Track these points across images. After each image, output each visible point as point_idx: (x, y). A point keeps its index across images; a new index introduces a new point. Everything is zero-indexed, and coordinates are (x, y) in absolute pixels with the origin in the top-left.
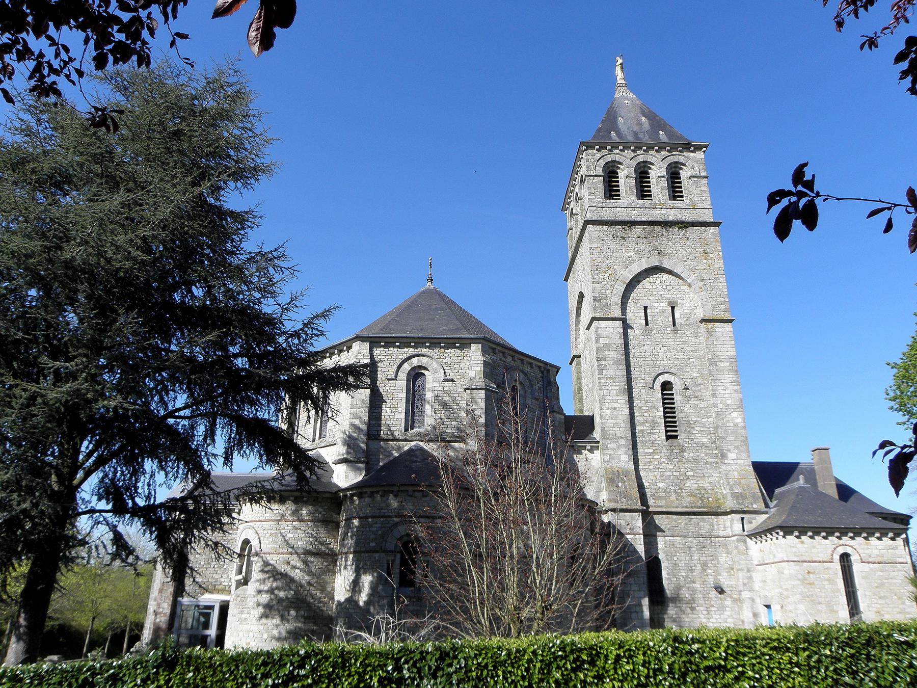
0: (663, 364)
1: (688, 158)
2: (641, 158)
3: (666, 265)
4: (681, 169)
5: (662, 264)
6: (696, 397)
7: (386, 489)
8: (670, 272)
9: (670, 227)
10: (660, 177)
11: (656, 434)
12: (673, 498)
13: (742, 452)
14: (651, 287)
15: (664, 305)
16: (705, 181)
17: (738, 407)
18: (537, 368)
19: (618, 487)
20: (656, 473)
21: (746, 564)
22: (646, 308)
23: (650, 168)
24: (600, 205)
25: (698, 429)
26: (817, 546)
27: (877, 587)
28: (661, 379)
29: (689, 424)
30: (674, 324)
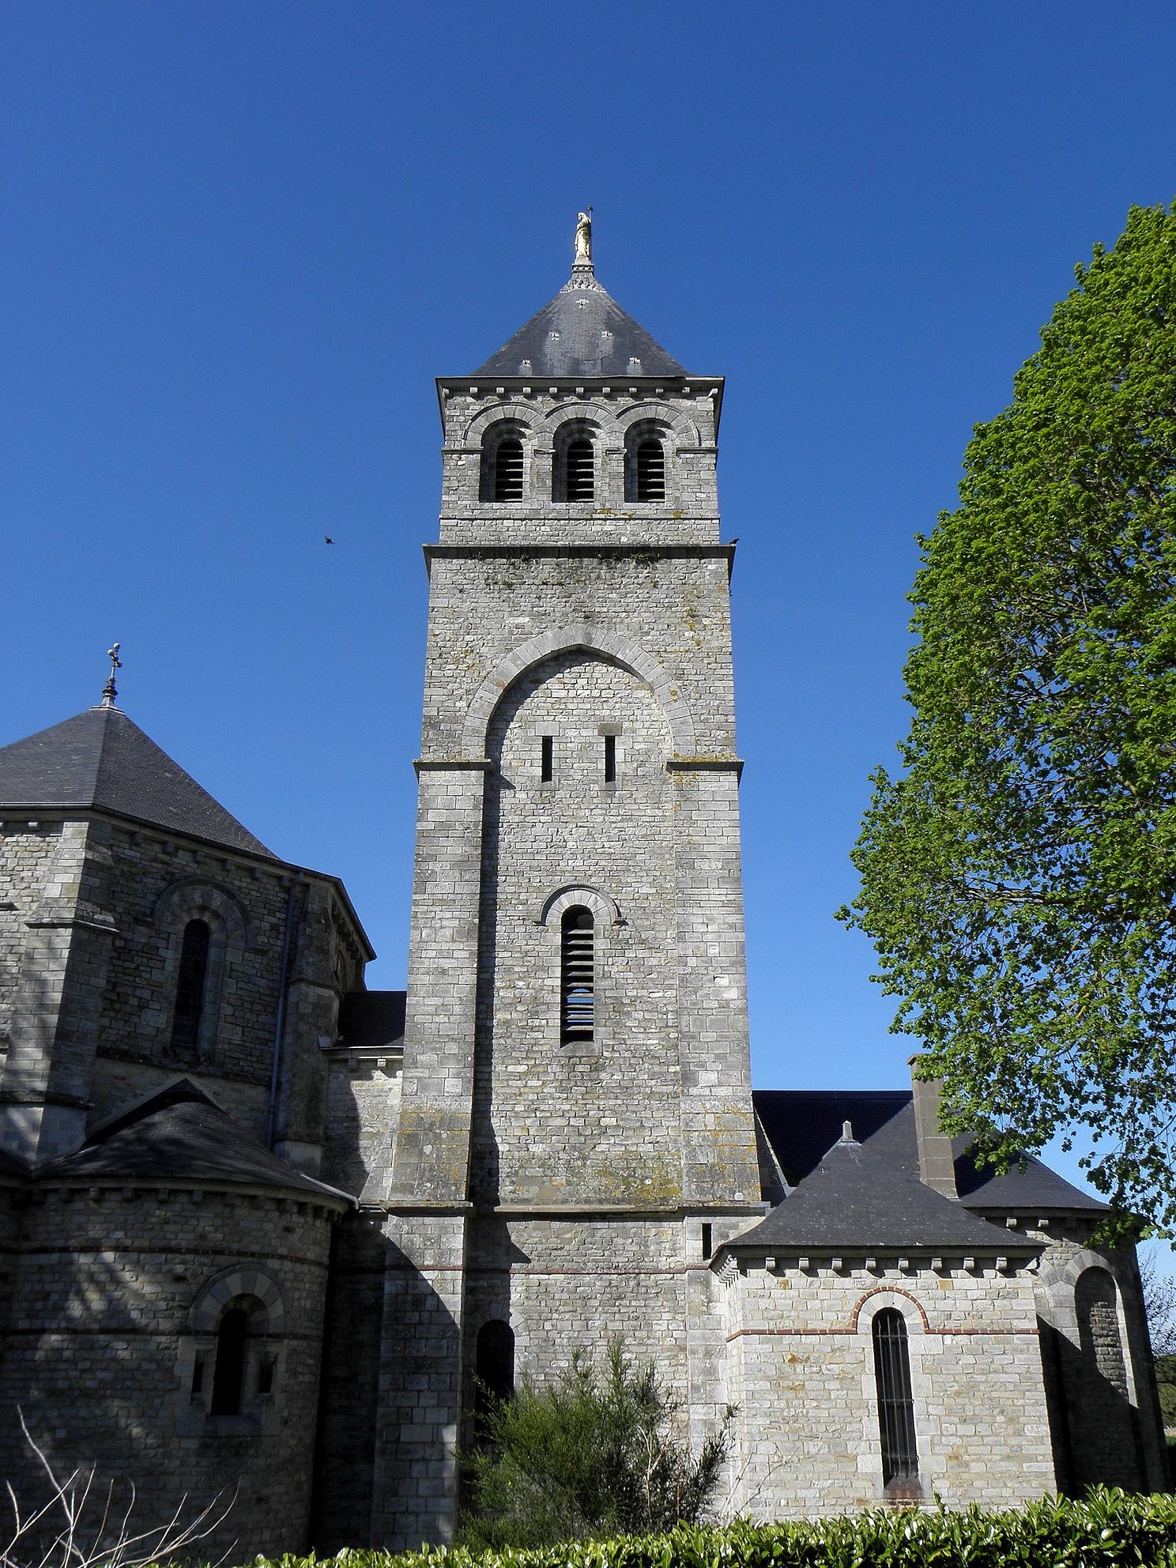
0: (574, 866)
1: (677, 410)
2: (570, 413)
3: (599, 643)
4: (663, 435)
5: (591, 640)
6: (643, 942)
7: (105, 1185)
8: (611, 660)
9: (618, 559)
10: (610, 452)
11: (539, 1029)
12: (560, 1180)
13: (732, 1067)
14: (564, 693)
15: (591, 733)
16: (710, 459)
17: (733, 964)
18: (273, 882)
19: (421, 1153)
20: (528, 1122)
21: (704, 1338)
22: (547, 742)
23: (593, 435)
24: (466, 514)
25: (639, 1015)
26: (823, 1294)
27: (958, 1394)
28: (566, 902)
29: (618, 1006)
30: (610, 775)
